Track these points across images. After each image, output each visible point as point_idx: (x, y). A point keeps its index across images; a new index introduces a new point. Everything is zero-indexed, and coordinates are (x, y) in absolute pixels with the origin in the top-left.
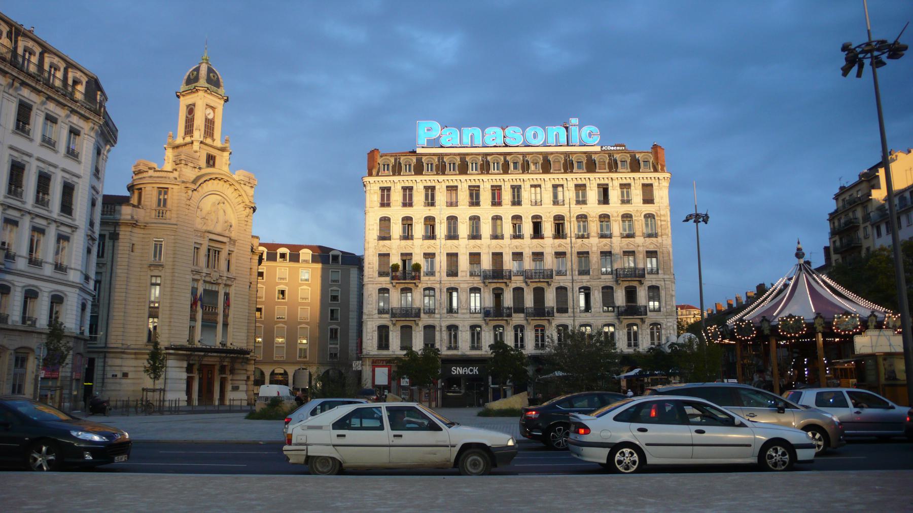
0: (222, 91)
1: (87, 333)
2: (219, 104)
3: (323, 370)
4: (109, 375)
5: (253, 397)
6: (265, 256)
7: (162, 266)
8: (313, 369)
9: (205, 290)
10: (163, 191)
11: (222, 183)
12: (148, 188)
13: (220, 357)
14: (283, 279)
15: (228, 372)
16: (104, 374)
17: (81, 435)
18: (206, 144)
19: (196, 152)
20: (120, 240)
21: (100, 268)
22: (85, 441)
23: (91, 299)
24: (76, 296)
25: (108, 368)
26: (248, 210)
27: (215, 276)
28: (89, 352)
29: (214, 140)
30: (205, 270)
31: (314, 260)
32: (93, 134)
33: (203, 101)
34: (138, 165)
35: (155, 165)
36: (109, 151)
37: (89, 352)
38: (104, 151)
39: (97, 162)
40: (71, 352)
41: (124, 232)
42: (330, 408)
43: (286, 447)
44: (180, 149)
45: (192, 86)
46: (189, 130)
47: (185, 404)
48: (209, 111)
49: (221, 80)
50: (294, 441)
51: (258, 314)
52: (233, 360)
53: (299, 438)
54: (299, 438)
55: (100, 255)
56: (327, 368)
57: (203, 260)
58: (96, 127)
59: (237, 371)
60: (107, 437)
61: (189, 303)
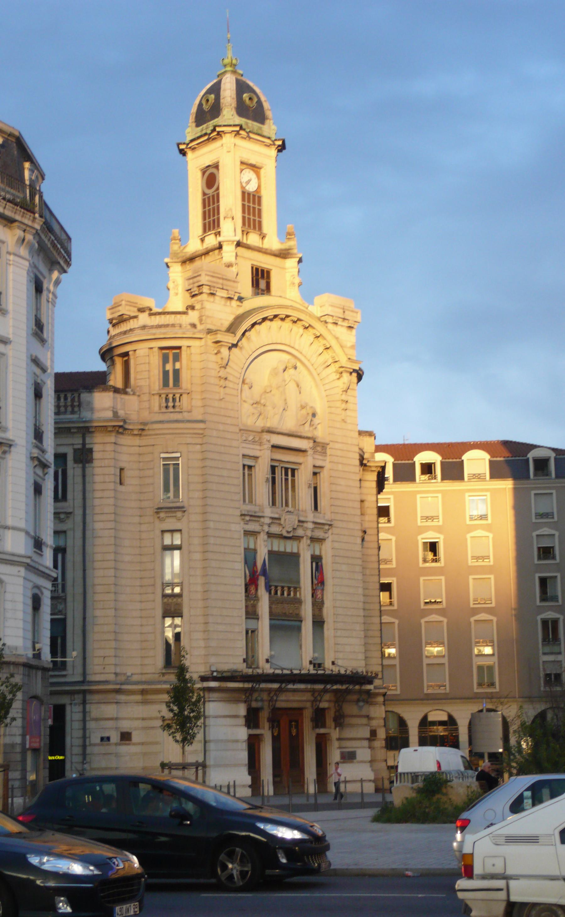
0: (270, 128)
1: (46, 655)
2: (267, 157)
3: (531, 712)
4: (95, 738)
5: (385, 774)
6: (389, 473)
7: (181, 509)
8: (511, 711)
9: (270, 553)
10: (171, 353)
11: (287, 324)
12: (142, 350)
13: (313, 691)
14: (432, 518)
15: (330, 721)
16: (84, 737)
17: (50, 863)
18: (248, 247)
19: (229, 265)
20: (96, 463)
21: (62, 521)
22: (55, 875)
23: (48, 585)
24: (21, 581)
25: (91, 725)
26: (346, 376)
27: (289, 521)
28: (53, 693)
29: (263, 237)
30: (268, 512)
31: (496, 472)
32: (23, 251)
33: (239, 159)
34: (117, 305)
35: (150, 302)
36: (57, 282)
37: (53, 693)
38: (49, 285)
39: (38, 309)
40: (19, 695)
41: (101, 446)
42: (553, 796)
43: (462, 883)
44: (197, 263)
45: (208, 127)
46: (211, 222)
47: (247, 792)
48: (249, 174)
49: (266, 105)
50: (478, 870)
51: (384, 596)
52: (340, 698)
53: (489, 862)
54: (489, 862)
55: (61, 495)
56: (540, 707)
57: (262, 491)
58: (29, 237)
59: (347, 720)
60: (97, 866)
61: (241, 582)
